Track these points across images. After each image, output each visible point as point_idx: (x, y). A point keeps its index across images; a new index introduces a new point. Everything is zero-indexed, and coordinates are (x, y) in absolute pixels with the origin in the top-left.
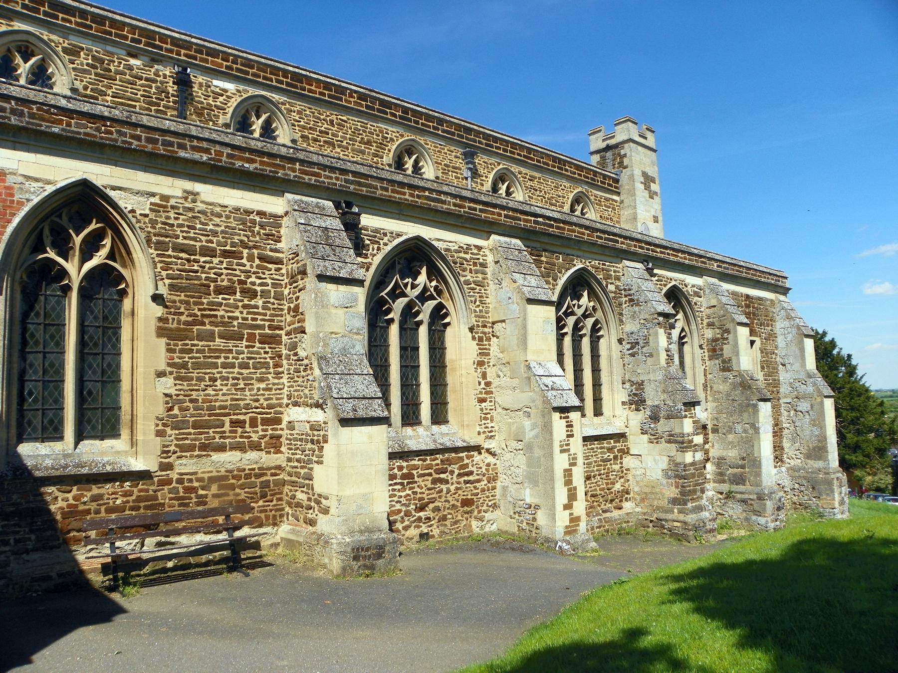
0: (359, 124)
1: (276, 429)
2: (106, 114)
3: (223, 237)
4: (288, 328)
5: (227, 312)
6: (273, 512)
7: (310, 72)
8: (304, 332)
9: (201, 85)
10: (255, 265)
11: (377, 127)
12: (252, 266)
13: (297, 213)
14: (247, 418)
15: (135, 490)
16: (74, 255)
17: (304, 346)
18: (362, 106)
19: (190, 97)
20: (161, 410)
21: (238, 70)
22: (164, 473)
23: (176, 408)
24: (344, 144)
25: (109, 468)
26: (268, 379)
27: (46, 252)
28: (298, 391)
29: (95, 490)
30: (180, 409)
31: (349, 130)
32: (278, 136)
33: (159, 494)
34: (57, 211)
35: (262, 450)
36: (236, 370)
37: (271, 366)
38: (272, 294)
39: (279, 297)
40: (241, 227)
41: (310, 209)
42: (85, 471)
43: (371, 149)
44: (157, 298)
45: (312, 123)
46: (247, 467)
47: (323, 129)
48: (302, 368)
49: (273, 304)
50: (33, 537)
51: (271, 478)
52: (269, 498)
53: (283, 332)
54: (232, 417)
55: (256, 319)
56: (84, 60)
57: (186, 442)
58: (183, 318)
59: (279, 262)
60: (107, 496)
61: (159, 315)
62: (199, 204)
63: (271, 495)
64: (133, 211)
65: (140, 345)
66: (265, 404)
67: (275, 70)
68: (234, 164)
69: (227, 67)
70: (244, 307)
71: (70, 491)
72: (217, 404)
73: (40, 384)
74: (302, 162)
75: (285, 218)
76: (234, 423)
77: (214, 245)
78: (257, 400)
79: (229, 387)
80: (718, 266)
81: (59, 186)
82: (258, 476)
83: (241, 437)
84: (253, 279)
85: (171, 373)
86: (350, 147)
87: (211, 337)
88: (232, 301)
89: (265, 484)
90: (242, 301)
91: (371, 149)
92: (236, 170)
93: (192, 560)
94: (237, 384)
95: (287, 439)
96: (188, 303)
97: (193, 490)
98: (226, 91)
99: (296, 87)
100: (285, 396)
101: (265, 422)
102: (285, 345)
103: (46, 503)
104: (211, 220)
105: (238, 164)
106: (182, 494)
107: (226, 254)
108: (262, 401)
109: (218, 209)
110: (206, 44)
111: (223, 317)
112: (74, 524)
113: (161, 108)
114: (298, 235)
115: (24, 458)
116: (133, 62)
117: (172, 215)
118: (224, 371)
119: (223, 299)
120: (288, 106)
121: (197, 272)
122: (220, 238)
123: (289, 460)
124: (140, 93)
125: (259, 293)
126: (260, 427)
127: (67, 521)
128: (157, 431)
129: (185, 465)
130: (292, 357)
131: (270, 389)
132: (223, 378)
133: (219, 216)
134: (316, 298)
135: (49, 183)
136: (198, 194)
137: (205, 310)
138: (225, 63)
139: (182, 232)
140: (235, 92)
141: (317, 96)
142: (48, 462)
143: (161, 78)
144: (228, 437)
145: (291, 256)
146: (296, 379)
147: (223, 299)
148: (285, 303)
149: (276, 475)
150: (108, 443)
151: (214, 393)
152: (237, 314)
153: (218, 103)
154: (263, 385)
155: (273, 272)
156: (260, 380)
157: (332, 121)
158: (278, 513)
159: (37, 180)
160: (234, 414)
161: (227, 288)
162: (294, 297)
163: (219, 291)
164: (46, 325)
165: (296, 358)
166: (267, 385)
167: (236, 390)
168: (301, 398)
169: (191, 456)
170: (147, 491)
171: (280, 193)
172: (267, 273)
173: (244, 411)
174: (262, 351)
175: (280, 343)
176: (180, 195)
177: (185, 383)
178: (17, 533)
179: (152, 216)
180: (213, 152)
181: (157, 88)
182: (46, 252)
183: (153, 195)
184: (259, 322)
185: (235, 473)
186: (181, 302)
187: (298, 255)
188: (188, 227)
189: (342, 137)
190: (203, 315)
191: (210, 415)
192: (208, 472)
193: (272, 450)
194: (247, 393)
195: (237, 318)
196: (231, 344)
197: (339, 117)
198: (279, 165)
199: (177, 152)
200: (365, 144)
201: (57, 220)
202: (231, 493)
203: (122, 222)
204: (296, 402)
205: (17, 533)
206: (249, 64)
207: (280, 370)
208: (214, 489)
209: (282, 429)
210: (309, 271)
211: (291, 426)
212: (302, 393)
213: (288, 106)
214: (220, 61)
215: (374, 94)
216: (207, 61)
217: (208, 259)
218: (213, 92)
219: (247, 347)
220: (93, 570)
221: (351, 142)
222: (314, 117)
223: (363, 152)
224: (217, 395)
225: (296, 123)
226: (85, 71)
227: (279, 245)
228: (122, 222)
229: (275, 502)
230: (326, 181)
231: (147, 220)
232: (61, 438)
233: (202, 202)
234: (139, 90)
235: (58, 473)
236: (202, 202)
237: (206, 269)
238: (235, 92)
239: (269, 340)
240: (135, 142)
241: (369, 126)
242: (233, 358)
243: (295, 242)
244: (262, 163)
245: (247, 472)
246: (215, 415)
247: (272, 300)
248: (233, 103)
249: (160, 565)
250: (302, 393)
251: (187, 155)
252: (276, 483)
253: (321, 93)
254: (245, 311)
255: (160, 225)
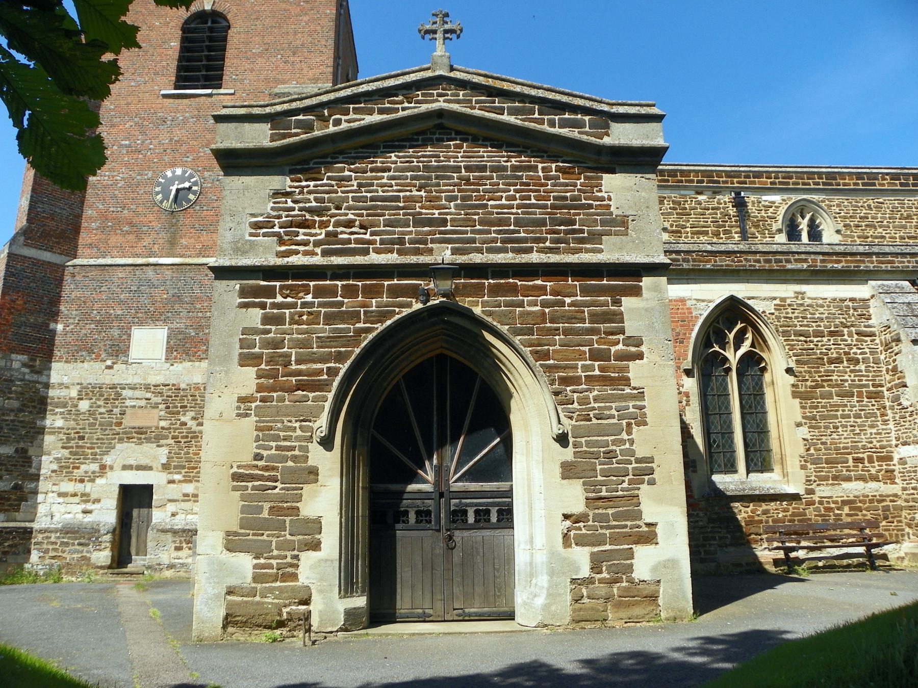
0: (896, 202)
1: (890, 465)
2: (736, 249)
3: (828, 322)
4: (889, 385)
5: (839, 376)
6: (895, 532)
7: (841, 168)
8: (905, 386)
9: (753, 203)
10: (854, 339)
11: (915, 200)
12: (852, 341)
13: (882, 295)
14: (865, 456)
15: (790, 507)
16: (730, 347)
17: (907, 397)
18: (896, 185)
19: (747, 215)
20: (802, 450)
21: (780, 183)
22: (809, 496)
23: (812, 448)
24: (885, 223)
25: (772, 492)
26: (877, 426)
27: (714, 347)
28: (907, 433)
29: (764, 506)
30: (815, 450)
31: (887, 210)
32: (823, 230)
33: (807, 511)
34: (716, 320)
35: (880, 481)
36: (852, 419)
37: (879, 415)
38: (871, 360)
39: (877, 361)
40: (839, 312)
41: (892, 290)
42: (757, 492)
43: (912, 222)
44: (789, 371)
45: (852, 211)
46: (870, 494)
47: (862, 215)
48: (907, 415)
49: (873, 367)
50: (729, 536)
51: (891, 504)
52: (890, 519)
53: (884, 389)
54: (853, 455)
55: (861, 380)
56: (667, 205)
57: (822, 474)
58: (809, 383)
59: (872, 335)
60: (772, 511)
61: (792, 382)
62: (806, 300)
63: (892, 517)
64: (764, 312)
65: (782, 405)
66: (878, 445)
67: (811, 175)
68: (827, 267)
69: (771, 183)
70: (851, 371)
71: (748, 507)
72: (841, 445)
73: (720, 435)
74: (877, 254)
75: (871, 300)
76: (856, 460)
77: (822, 328)
78: (871, 442)
79: (848, 432)
80: (455, 252)
81: (718, 302)
82: (879, 501)
83: (862, 471)
84: (855, 350)
85: (806, 424)
86: (891, 225)
87: (829, 396)
88: (841, 368)
89: (887, 508)
90: (849, 367)
91: (912, 222)
92: (829, 270)
93: (836, 562)
94: (854, 430)
95: (900, 473)
96: (810, 372)
97: (831, 509)
98: (774, 202)
99: (831, 184)
100: (894, 439)
101: (880, 459)
102: (888, 399)
103: (734, 514)
104: (817, 310)
105: (829, 266)
106: (823, 513)
107: (832, 334)
108: (875, 443)
109: (821, 302)
110: (752, 169)
111: (836, 380)
112: (753, 530)
113: (727, 228)
114: (888, 312)
115: (717, 484)
116: (701, 198)
117: (790, 311)
118: (843, 420)
119: (835, 367)
120: (827, 202)
121: (813, 349)
122: (826, 323)
123: (904, 489)
124: (709, 220)
125: (861, 361)
126: (876, 464)
127: (749, 527)
128: (801, 466)
129: (823, 491)
130: (896, 407)
131: (880, 434)
132: (843, 426)
133: (822, 306)
134: (913, 358)
135: (710, 302)
136: (804, 293)
137: (822, 376)
138: (769, 180)
139: (798, 321)
140: (781, 201)
141: (852, 187)
142: (732, 487)
143: (723, 205)
144: (853, 471)
145: (883, 329)
146: (903, 423)
147: (835, 367)
148: (882, 365)
149: (894, 501)
150: (766, 475)
151: (838, 437)
152: (847, 377)
153: (770, 214)
154: (874, 431)
155: (869, 343)
156: (872, 426)
157: (869, 206)
158: (900, 533)
159: (703, 301)
160: (855, 453)
161: (837, 358)
162: (891, 360)
163: (831, 362)
164: (718, 395)
165: (900, 407)
166: (877, 430)
167: (854, 434)
168: (910, 438)
169: (827, 484)
170: (798, 509)
171: (865, 282)
172: (864, 344)
173: (862, 450)
174: (870, 404)
175: (883, 397)
176: (793, 296)
177: (816, 431)
178: (720, 532)
179: (777, 313)
180: (810, 260)
181: (721, 213)
182: (714, 347)
183: (775, 299)
184: (864, 382)
185: (861, 498)
186: (805, 372)
187: (889, 328)
188: (802, 317)
189: (881, 218)
190: (822, 381)
191: (837, 454)
192: (841, 497)
193: (889, 481)
194: (863, 437)
195: (847, 381)
196: (845, 400)
197: (876, 200)
198: (860, 260)
199: (785, 266)
200: (906, 218)
201: (717, 325)
202: (860, 514)
203: (759, 321)
204: (906, 442)
205: (720, 532)
206: (788, 176)
207: (886, 418)
208: (846, 509)
209: (894, 465)
210: (903, 337)
211: (902, 461)
212: (911, 435)
213: (827, 202)
214: (765, 180)
215: (906, 171)
216: (754, 183)
217: (819, 339)
218: (764, 206)
219: (858, 402)
220: (768, 563)
221: (891, 221)
222: (852, 206)
223: (905, 227)
224: (840, 439)
225: (837, 215)
226: (669, 214)
227: (870, 322)
228: (759, 321)
229: (895, 524)
230: (900, 265)
231: (774, 317)
232: (736, 472)
233: (808, 298)
234: (709, 218)
235: (741, 493)
236: (808, 298)
237: (819, 346)
238: (781, 201)
239: (873, 395)
240: (758, 265)
241: (906, 202)
242: (849, 410)
243: (885, 318)
244: (847, 261)
245: (870, 498)
246: (841, 454)
247: (872, 365)
248: (782, 211)
249: (813, 564)
250: (911, 435)
251: (793, 267)
252: (895, 508)
253: (855, 184)
254: (852, 375)
255: (783, 319)
